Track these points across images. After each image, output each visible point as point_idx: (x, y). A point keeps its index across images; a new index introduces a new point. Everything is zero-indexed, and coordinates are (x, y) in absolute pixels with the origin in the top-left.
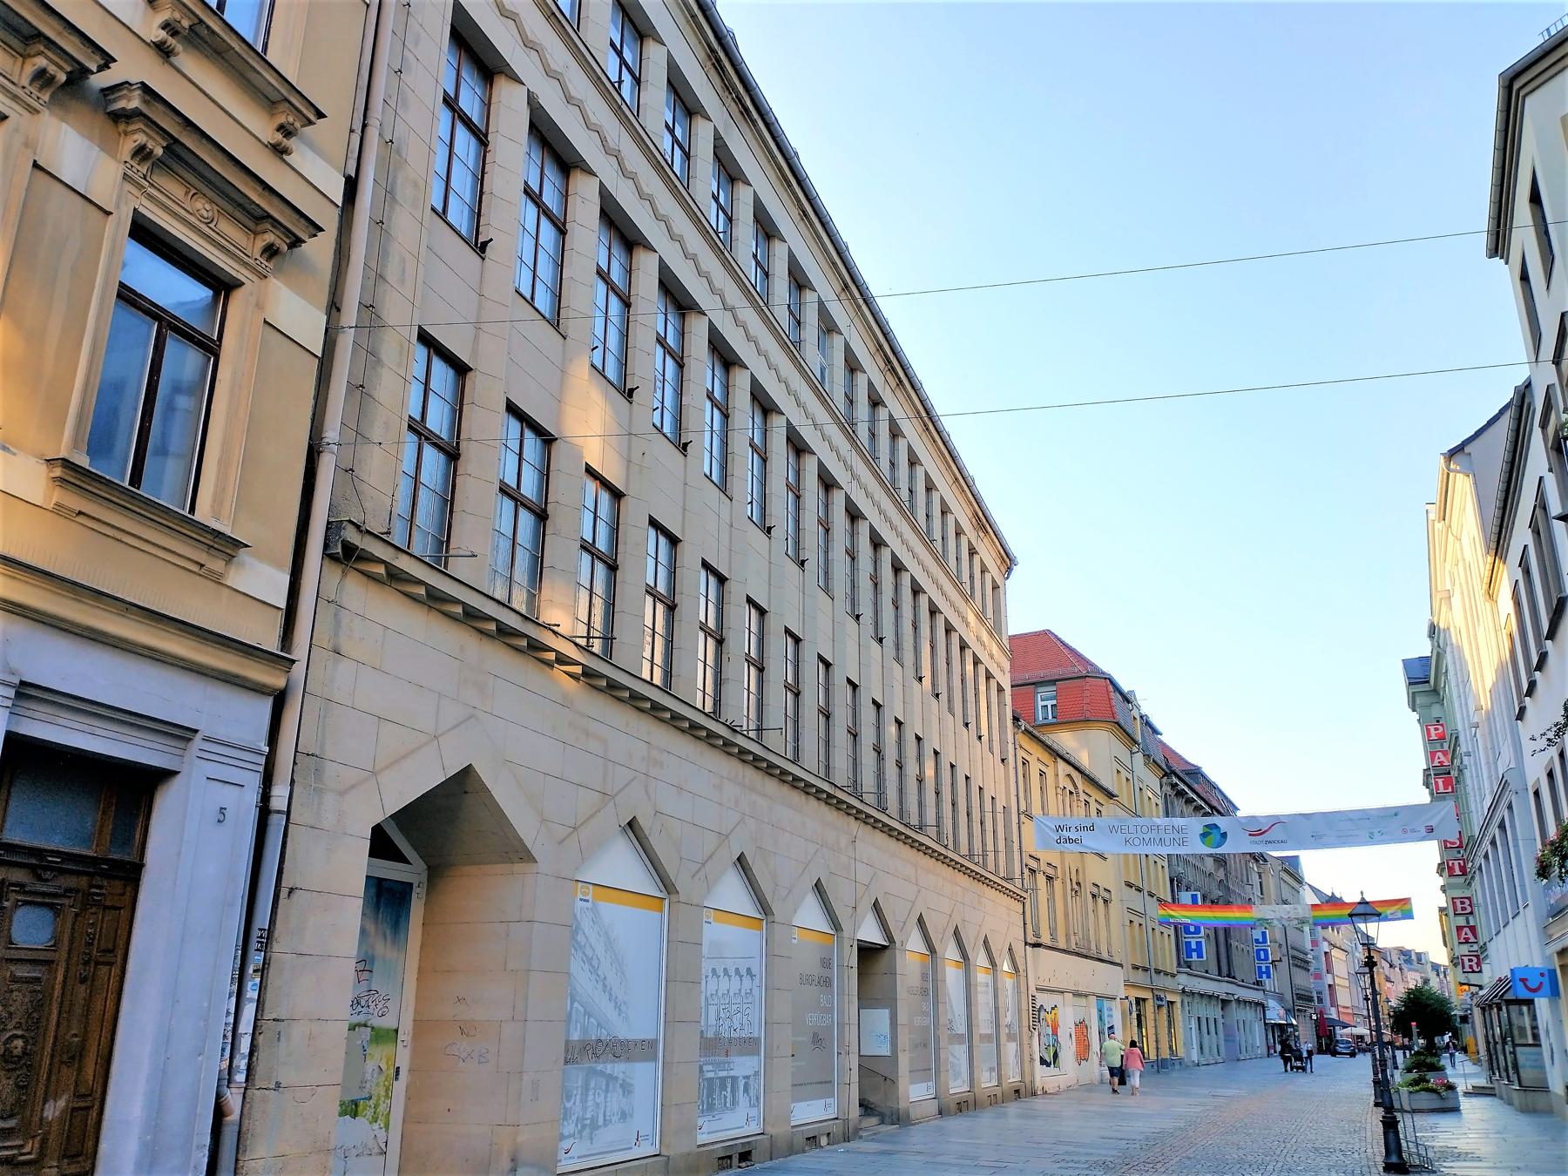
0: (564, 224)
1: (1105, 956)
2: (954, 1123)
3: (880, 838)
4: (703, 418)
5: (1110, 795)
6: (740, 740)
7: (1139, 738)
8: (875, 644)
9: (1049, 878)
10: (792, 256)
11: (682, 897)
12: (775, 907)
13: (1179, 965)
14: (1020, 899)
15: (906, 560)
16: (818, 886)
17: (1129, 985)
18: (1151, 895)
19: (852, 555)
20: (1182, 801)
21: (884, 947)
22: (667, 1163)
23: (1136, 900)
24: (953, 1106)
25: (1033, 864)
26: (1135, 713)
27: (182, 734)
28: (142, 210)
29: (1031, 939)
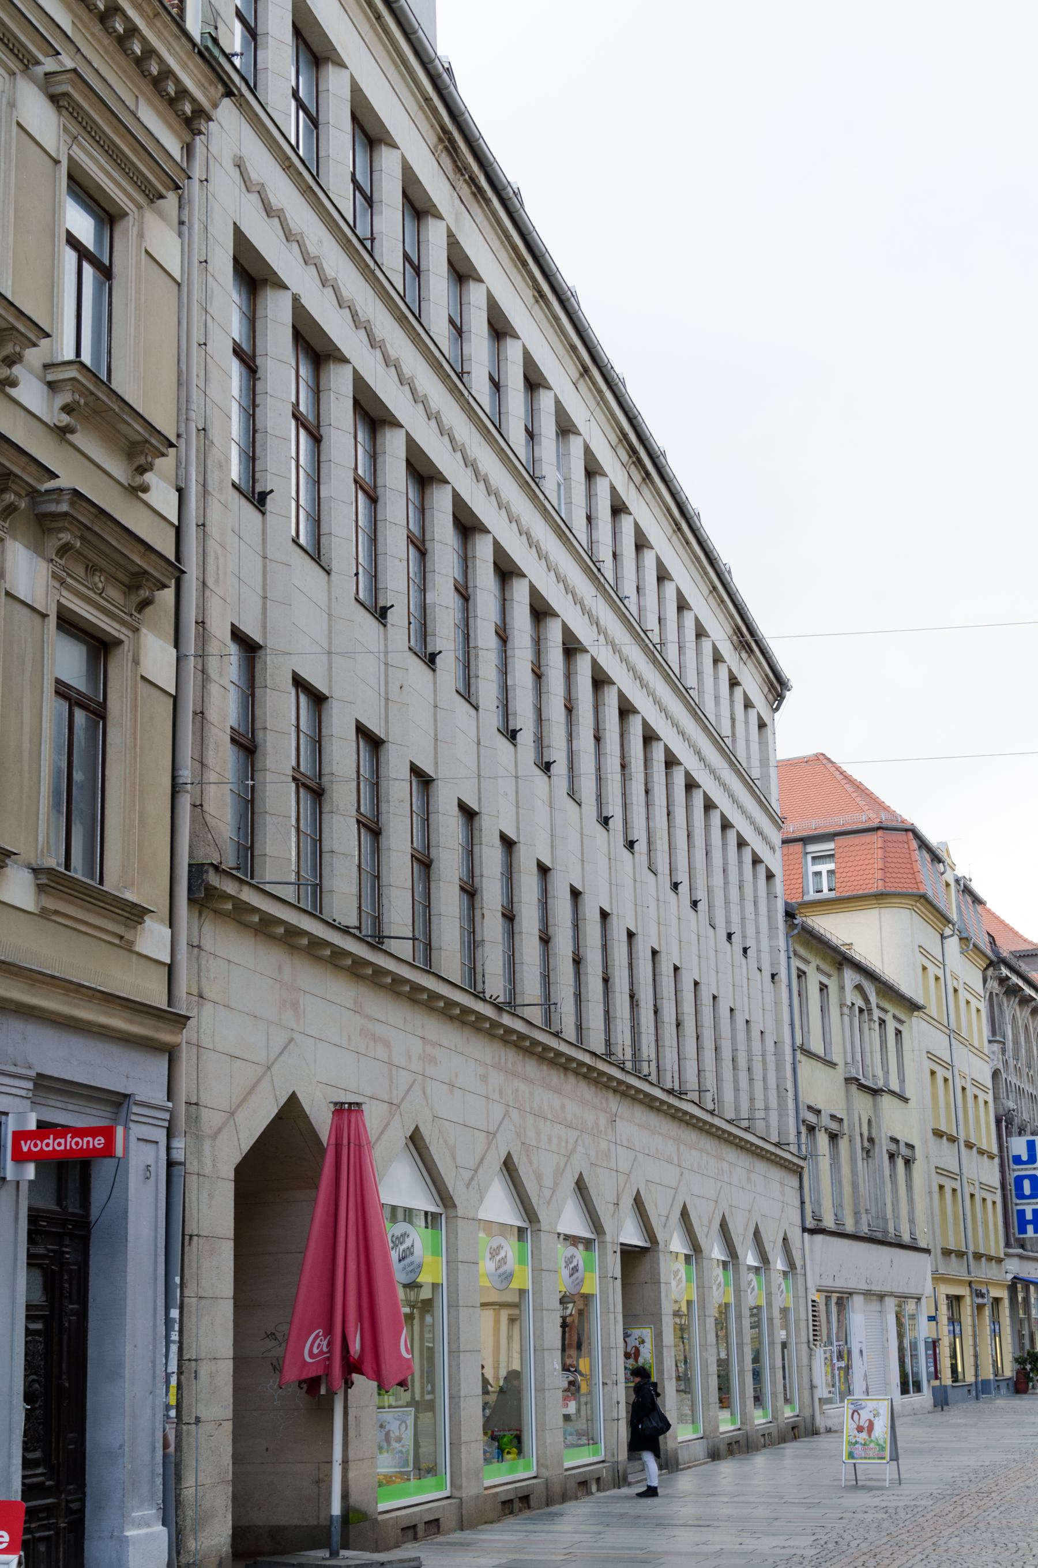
0: (424, 541)
1: (906, 1238)
2: (727, 1468)
3: (640, 1114)
4: (285, 451)
5: (913, 1007)
6: (506, 1020)
7: (954, 916)
8: (503, 743)
9: (833, 1137)
10: (356, 91)
11: (460, 1212)
12: (542, 1214)
13: (1008, 1245)
14: (799, 1172)
15: (555, 596)
16: (509, 1166)
17: (938, 1278)
18: (969, 1145)
19: (464, 593)
20: (1014, 1002)
21: (644, 1250)
22: (461, 1503)
23: (947, 1156)
24: (723, 1447)
25: (811, 1118)
26: (949, 877)
27: (118, 1102)
28: (63, 601)
29: (810, 1224)
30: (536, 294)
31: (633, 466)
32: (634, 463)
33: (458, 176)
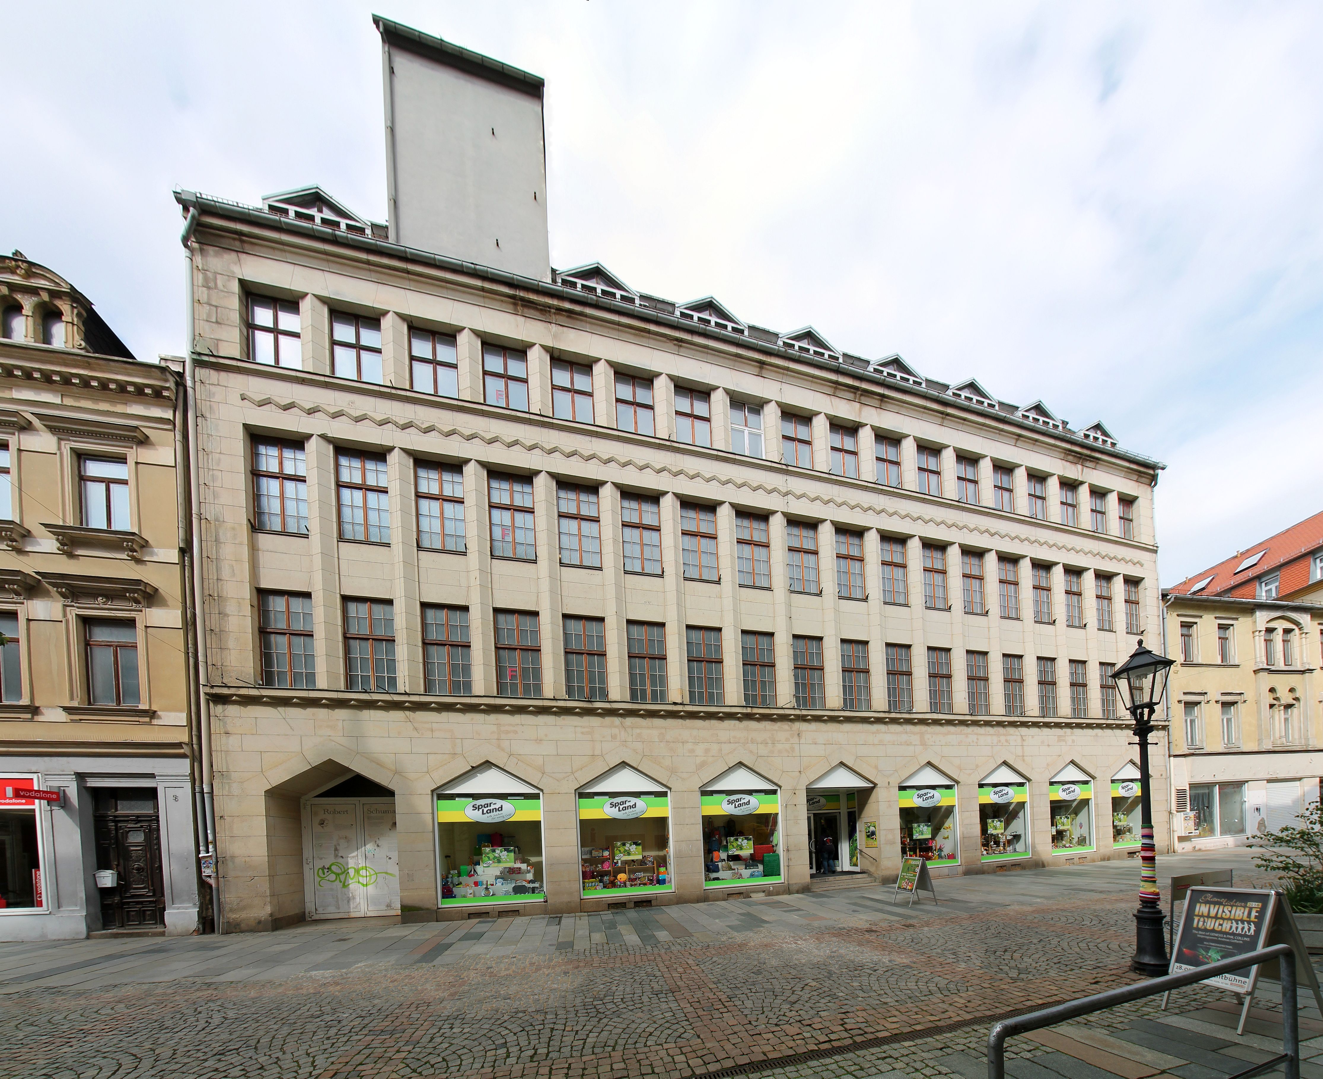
30: (675, 342)
31: (862, 398)
32: (861, 395)
33: (547, 315)
